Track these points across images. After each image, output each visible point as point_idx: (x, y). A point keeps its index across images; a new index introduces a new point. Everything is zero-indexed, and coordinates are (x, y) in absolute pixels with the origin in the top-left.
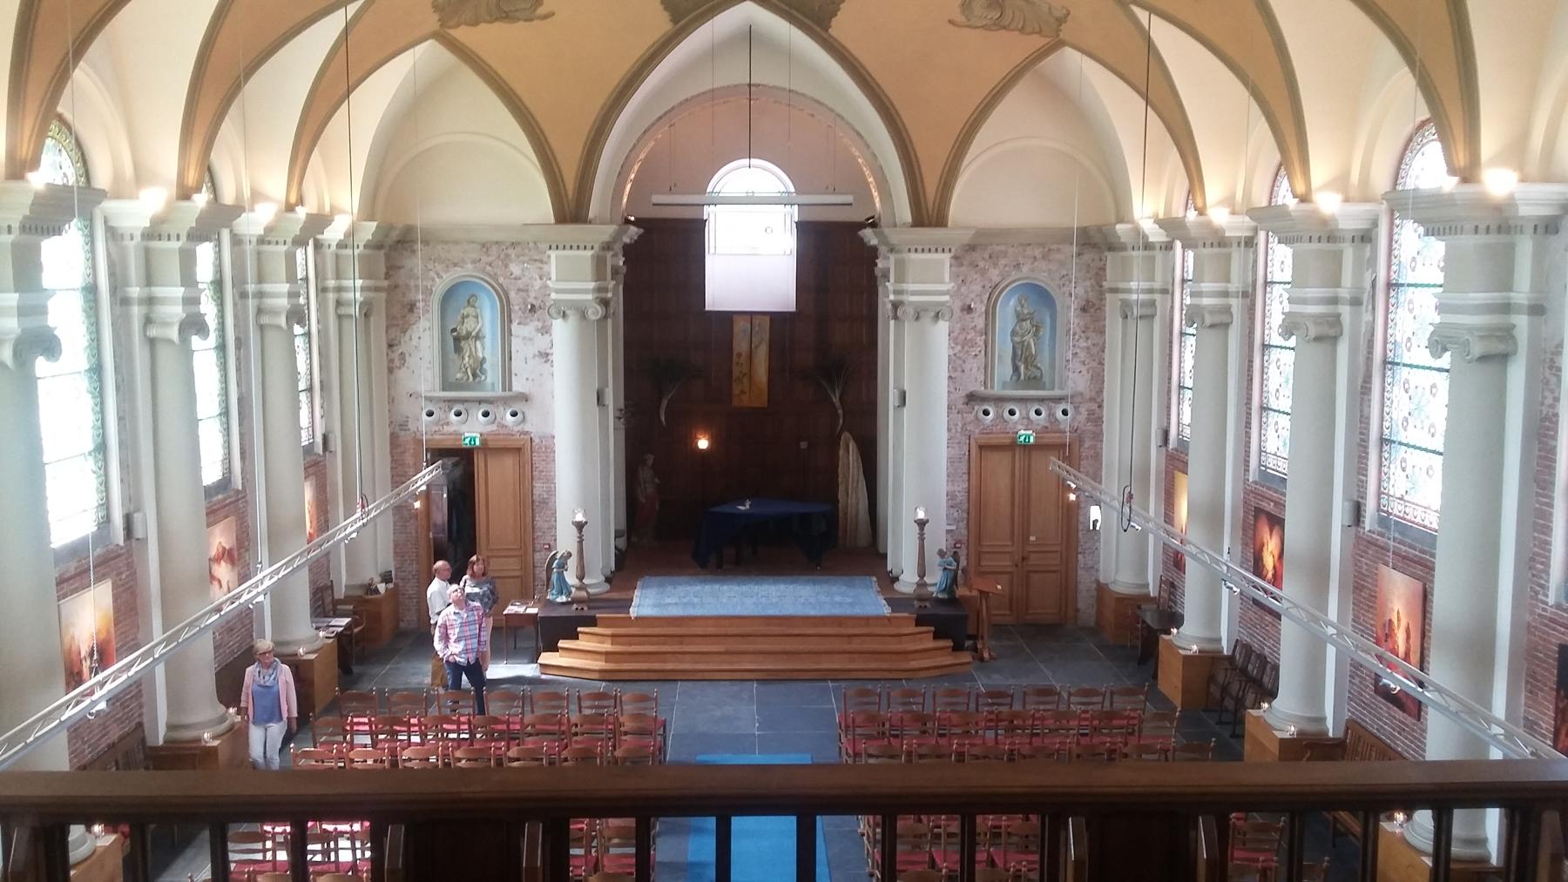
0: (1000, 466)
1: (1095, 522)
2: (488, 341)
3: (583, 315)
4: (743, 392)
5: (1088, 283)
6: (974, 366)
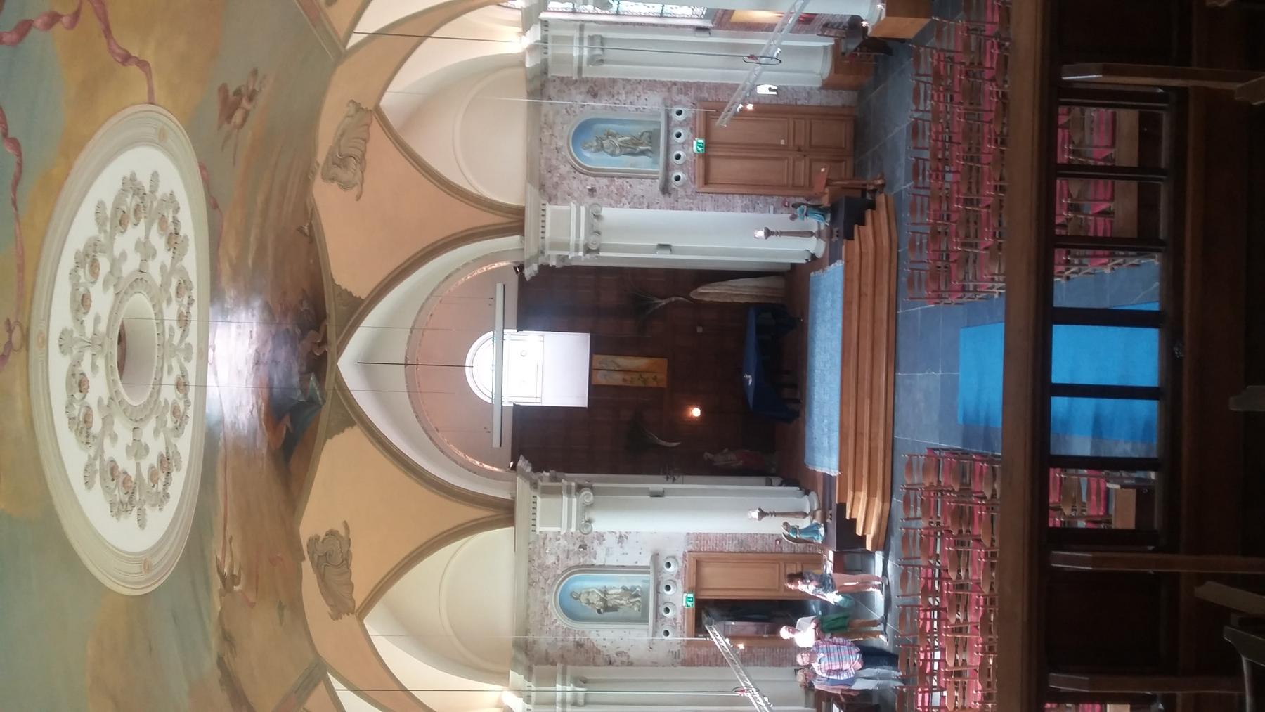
0: (721, 168)
1: (771, 90)
2: (608, 584)
3: (590, 506)
4: (655, 379)
5: (574, 91)
6: (640, 187)
